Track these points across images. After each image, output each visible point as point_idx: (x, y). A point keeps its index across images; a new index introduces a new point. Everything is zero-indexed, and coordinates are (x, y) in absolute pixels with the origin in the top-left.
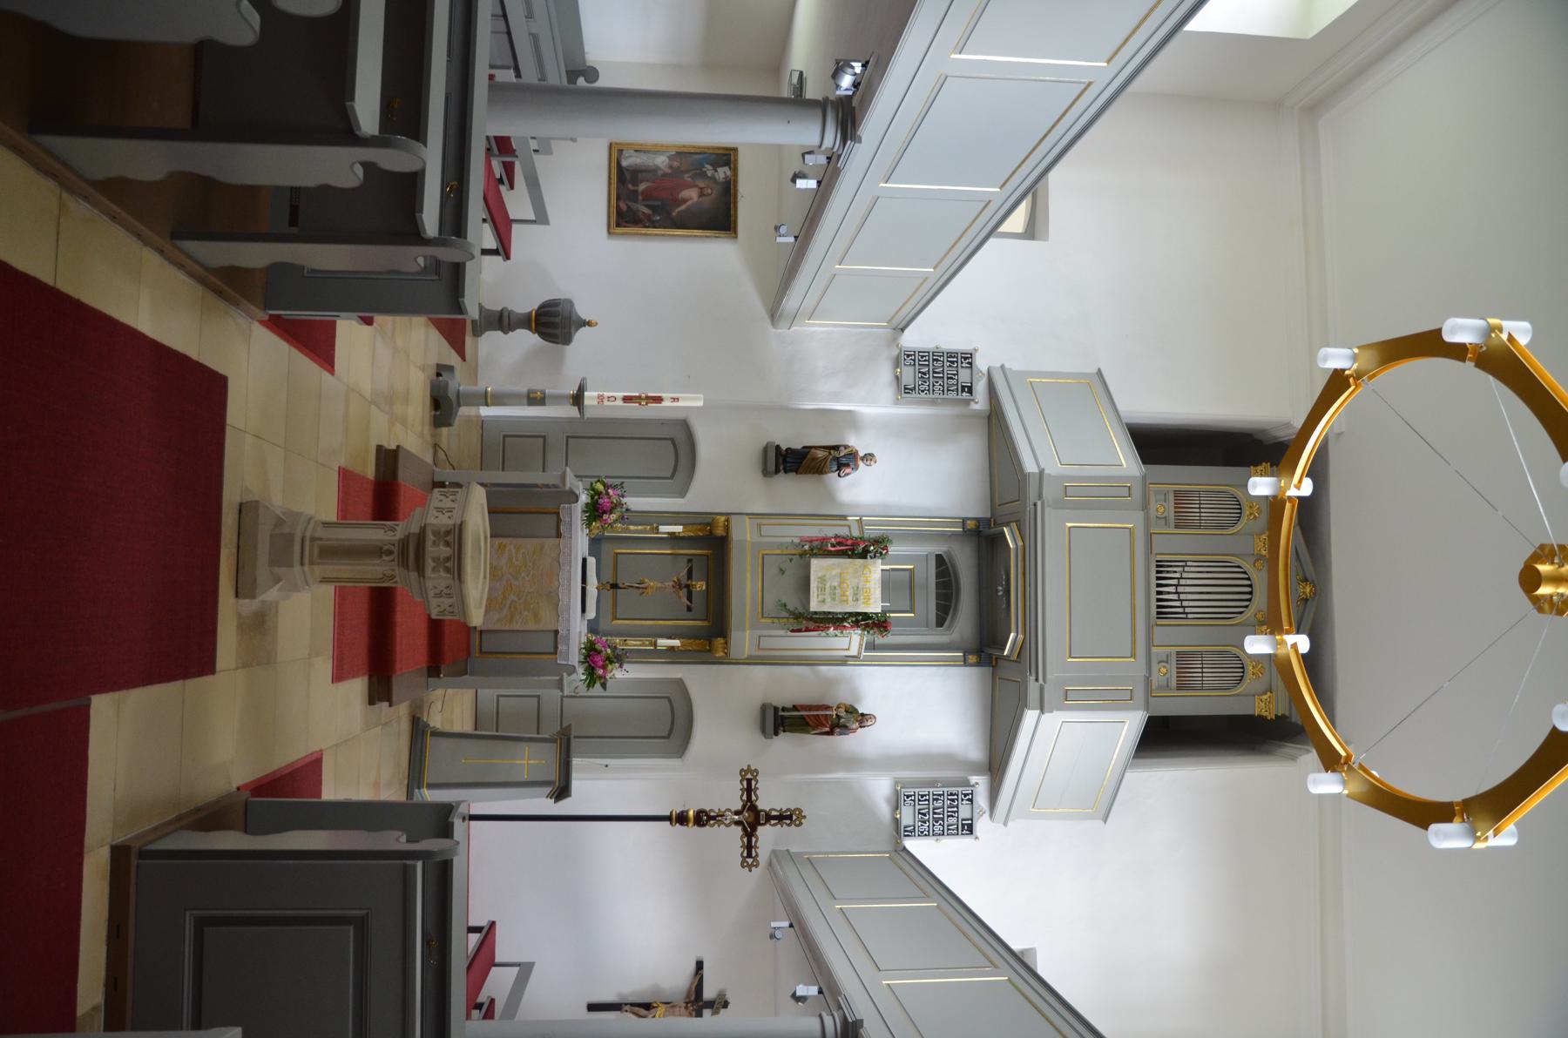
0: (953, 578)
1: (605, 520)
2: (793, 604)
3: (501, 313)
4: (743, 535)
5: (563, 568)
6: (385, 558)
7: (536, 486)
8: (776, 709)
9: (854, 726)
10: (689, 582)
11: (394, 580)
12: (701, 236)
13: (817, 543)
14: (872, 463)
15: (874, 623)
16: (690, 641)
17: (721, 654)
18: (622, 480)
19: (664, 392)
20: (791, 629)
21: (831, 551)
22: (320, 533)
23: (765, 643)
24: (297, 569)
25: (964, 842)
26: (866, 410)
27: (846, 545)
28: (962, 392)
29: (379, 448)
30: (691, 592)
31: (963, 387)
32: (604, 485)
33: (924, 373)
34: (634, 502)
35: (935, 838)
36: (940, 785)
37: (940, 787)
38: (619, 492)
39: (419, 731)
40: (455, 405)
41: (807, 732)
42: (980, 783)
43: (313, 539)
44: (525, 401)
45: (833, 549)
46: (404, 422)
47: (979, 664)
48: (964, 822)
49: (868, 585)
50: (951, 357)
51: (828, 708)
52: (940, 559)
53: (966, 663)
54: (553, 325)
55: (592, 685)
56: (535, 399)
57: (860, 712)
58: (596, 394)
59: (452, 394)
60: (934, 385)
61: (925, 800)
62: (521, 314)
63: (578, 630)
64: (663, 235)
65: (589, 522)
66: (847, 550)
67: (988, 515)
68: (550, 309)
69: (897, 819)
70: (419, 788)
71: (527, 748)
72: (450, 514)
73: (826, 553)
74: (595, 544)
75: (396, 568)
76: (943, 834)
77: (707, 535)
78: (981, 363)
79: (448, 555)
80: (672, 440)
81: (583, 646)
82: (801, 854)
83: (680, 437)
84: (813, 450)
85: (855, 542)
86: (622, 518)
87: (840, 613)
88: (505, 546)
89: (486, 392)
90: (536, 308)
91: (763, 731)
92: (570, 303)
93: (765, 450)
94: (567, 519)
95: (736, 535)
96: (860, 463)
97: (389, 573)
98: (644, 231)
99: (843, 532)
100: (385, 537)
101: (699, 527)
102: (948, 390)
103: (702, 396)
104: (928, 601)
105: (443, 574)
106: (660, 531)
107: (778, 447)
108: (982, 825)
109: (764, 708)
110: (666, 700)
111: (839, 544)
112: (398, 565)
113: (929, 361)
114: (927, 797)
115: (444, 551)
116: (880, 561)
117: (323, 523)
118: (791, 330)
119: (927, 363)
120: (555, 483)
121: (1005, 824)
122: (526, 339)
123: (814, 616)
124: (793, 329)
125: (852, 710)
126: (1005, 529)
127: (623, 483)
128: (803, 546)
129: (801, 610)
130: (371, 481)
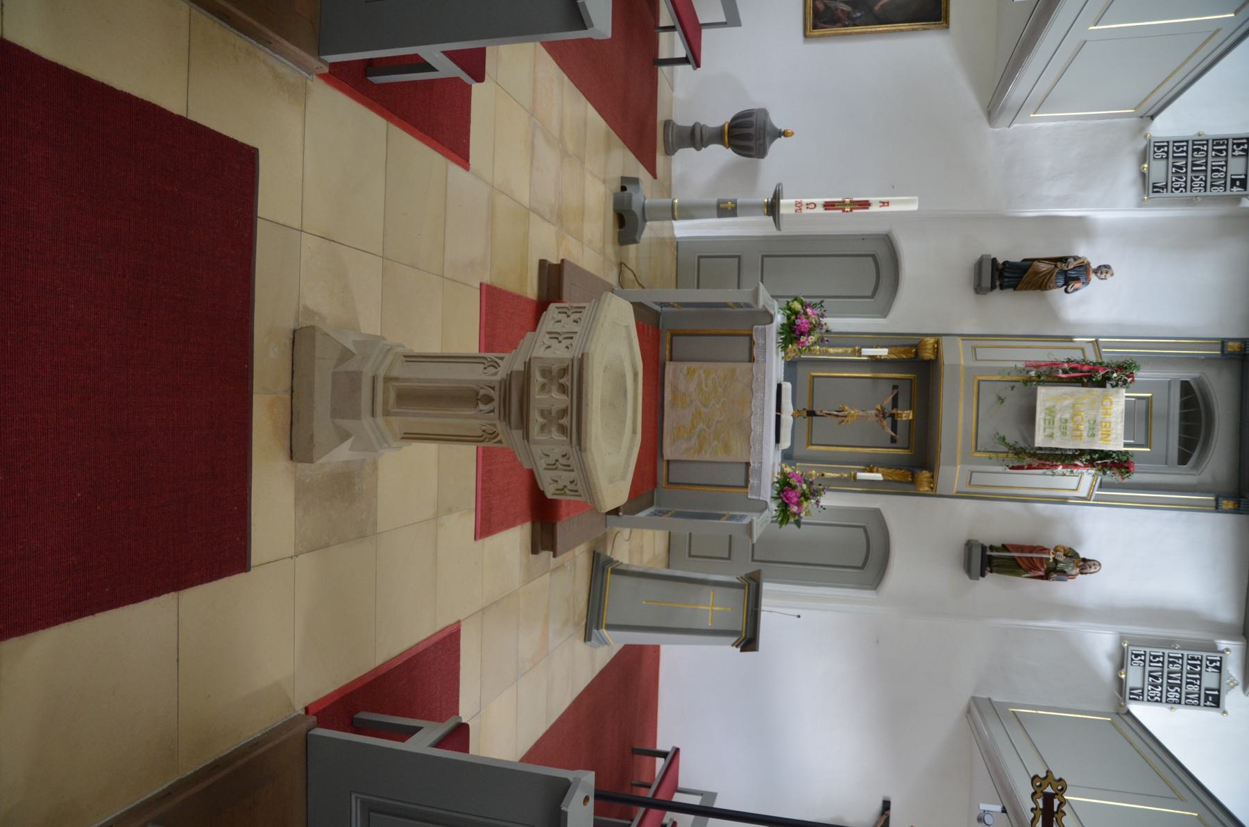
0: (1202, 408)
2: (1013, 436)
3: (693, 128)
4: (955, 357)
5: (755, 395)
6: (481, 407)
7: (725, 305)
8: (984, 548)
9: (1074, 572)
10: (894, 411)
11: (496, 440)
12: (908, 30)
13: (1045, 368)
14: (1108, 275)
15: (1112, 462)
16: (890, 471)
17: (927, 488)
18: (822, 299)
19: (871, 196)
20: (1011, 465)
21: (1061, 378)
22: (400, 371)
23: (977, 478)
24: (366, 421)
25: (1209, 714)
26: (1101, 215)
27: (1082, 372)
28: (1232, 187)
29: (543, 264)
30: (896, 421)
31: (1233, 182)
32: (802, 304)
33: (1180, 168)
34: (835, 323)
35: (1169, 706)
36: (1178, 646)
37: (1179, 649)
38: (818, 311)
39: (600, 567)
40: (640, 220)
41: (1019, 575)
43: (388, 379)
44: (715, 212)
45: (1064, 376)
46: (579, 238)
47: (1236, 511)
48: (1207, 692)
49: (1108, 418)
50: (1218, 144)
51: (1043, 550)
52: (1186, 387)
53: (1217, 508)
54: (747, 137)
55: (785, 521)
56: (726, 210)
58: (793, 201)
59: (636, 208)
60: (1192, 181)
61: (1159, 662)
62: (713, 128)
63: (771, 463)
64: (864, 33)
65: (784, 345)
66: (1081, 377)
68: (743, 120)
69: (1121, 680)
70: (598, 629)
71: (712, 593)
72: (569, 341)
73: (1056, 379)
74: (791, 367)
75: (497, 422)
77: (912, 358)
79: (564, 406)
80: (873, 256)
81: (776, 480)
82: (1006, 705)
83: (882, 253)
84: (1036, 263)
85: (1095, 367)
86: (821, 341)
87: (1070, 450)
88: (694, 371)
89: (673, 204)
90: (729, 121)
91: (968, 569)
92: (764, 112)
93: (980, 264)
94: (761, 341)
95: (947, 358)
96: (1093, 277)
97: (490, 429)
98: (843, 30)
99: (1077, 356)
100: (484, 377)
101: (903, 349)
102: (1212, 186)
103: (916, 198)
104: (1169, 435)
105: (556, 436)
106: (863, 354)
107: (994, 260)
108: (1233, 698)
109: (969, 545)
110: (862, 530)
112: (500, 418)
113: (1187, 152)
114: (1161, 659)
115: (558, 400)
116: (1124, 390)
117: (405, 356)
118: (1012, 128)
119: (1184, 154)
120: (746, 301)
122: (720, 154)
123: (1038, 452)
124: (1015, 125)
125: (1071, 555)
127: (822, 302)
128: (1028, 372)
129: (1022, 444)
130: (531, 301)
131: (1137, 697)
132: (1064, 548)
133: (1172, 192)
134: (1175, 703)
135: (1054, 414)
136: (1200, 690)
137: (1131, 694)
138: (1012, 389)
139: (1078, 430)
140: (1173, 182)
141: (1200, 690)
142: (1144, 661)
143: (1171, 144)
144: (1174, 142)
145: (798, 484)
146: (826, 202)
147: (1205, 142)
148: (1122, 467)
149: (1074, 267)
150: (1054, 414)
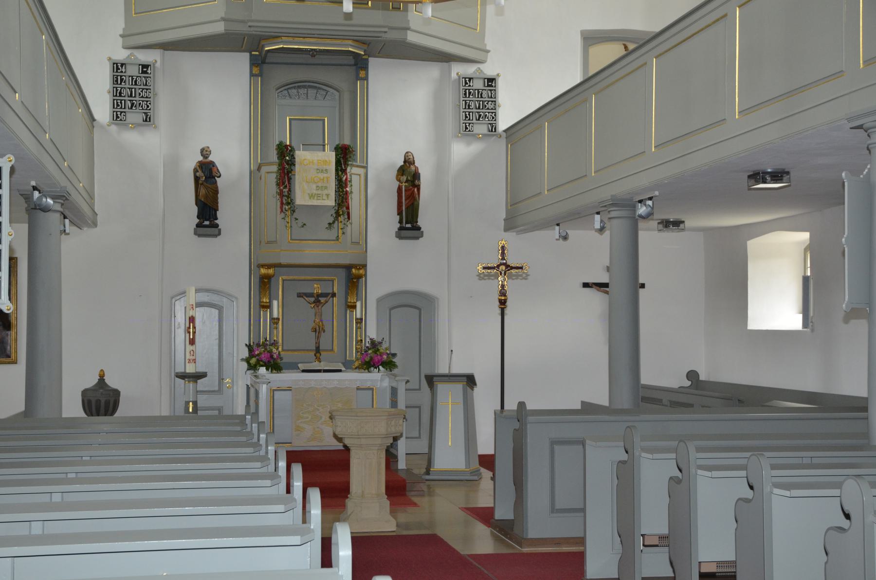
1: (277, 356)
8: (401, 229)
14: (208, 150)
15: (343, 158)
25: (501, 84)
28: (148, 73)
31: (143, 72)
33: (132, 104)
37: (460, 102)
42: (458, 70)
45: (288, 187)
50: (117, 81)
53: (366, 78)
54: (107, 403)
57: (403, 164)
60: (142, 97)
61: (469, 115)
67: (247, 55)
76: (495, 101)
78: (121, 55)
85: (281, 165)
91: (417, 238)
93: (200, 235)
96: (211, 158)
102: (146, 85)
108: (489, 70)
109: (399, 236)
110: (392, 311)
111: (283, 183)
113: (121, 100)
114: (467, 113)
121: (488, 51)
125: (402, 171)
126: (266, 49)
129: (333, 212)
131: (494, 127)
132: (397, 176)
133: (150, 109)
134: (495, 104)
135: (314, 195)
136: (485, 90)
137: (492, 131)
138: (297, 219)
139: (323, 179)
140: (143, 109)
141: (485, 90)
142: (470, 124)
143: (115, 110)
144: (114, 108)
145: (369, 356)
146: (190, 343)
147: (115, 89)
148: (346, 152)
149: (203, 172)
150: (314, 195)
